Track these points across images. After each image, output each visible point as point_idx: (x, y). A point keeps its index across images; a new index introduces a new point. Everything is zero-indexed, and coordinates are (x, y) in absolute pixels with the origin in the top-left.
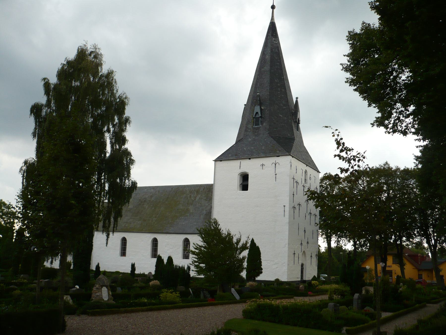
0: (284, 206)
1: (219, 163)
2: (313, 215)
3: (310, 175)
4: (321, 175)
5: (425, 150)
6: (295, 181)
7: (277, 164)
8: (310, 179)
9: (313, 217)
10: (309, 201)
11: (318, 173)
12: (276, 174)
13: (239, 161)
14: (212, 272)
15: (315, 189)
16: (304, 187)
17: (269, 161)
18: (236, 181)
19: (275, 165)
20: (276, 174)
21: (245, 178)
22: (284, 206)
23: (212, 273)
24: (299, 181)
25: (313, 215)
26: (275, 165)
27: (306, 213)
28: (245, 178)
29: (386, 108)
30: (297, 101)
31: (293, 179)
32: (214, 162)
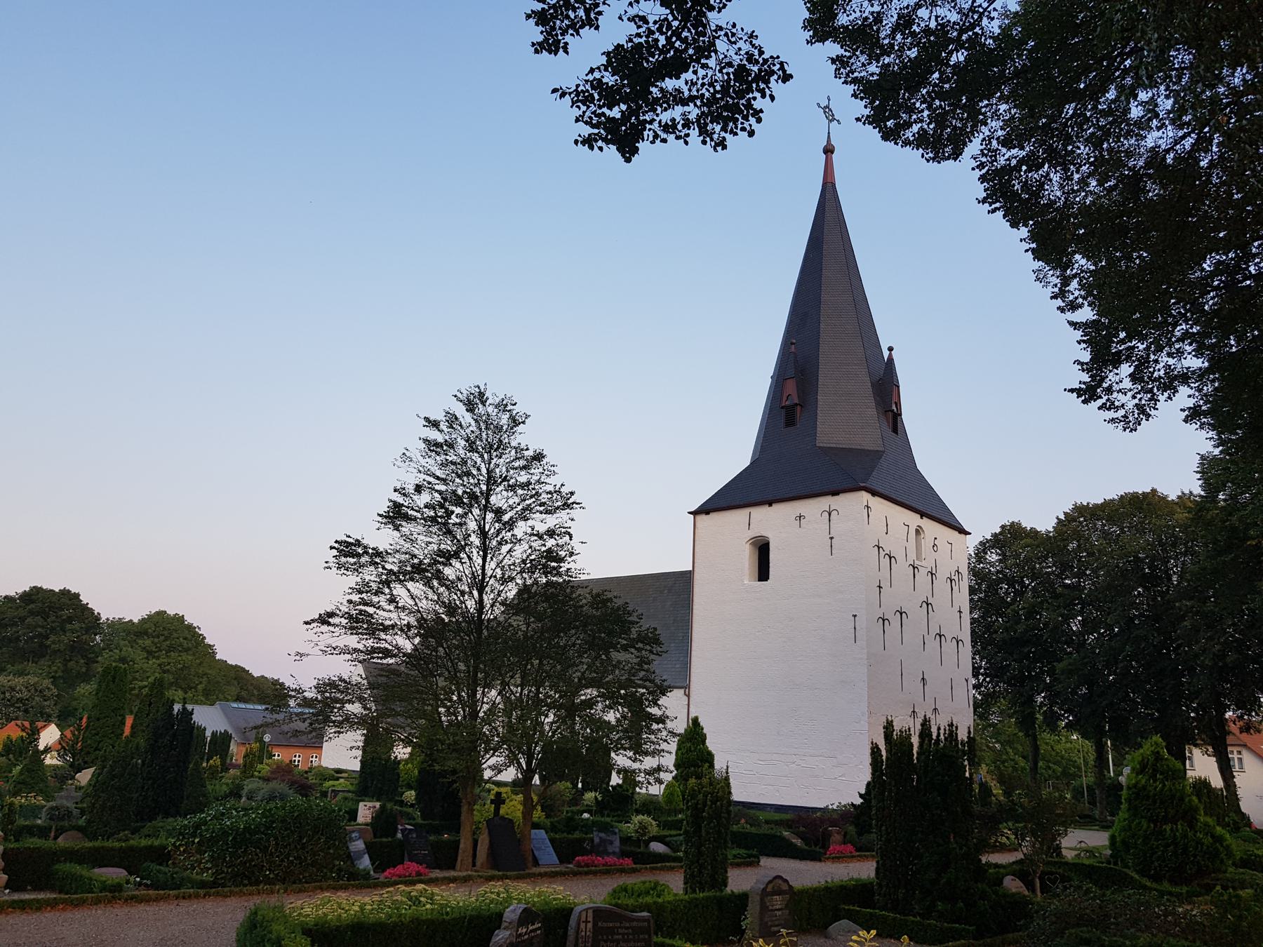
0: (855, 616)
1: (702, 518)
2: (949, 639)
3: (936, 538)
4: (972, 542)
5: (1033, 237)
6: (882, 553)
7: (834, 513)
8: (935, 548)
9: (950, 647)
10: (518, 538)
11: (963, 536)
12: (832, 538)
13: (745, 512)
14: (513, 760)
15: (953, 574)
16: (914, 568)
17: (813, 508)
18: (746, 559)
19: (830, 515)
20: (832, 538)
21: (762, 550)
22: (855, 616)
23: (498, 769)
24: (899, 554)
25: (949, 639)
26: (830, 515)
27: (926, 634)
28: (762, 550)
29: (674, 7)
30: (891, 359)
31: (876, 548)
32: (692, 516)
